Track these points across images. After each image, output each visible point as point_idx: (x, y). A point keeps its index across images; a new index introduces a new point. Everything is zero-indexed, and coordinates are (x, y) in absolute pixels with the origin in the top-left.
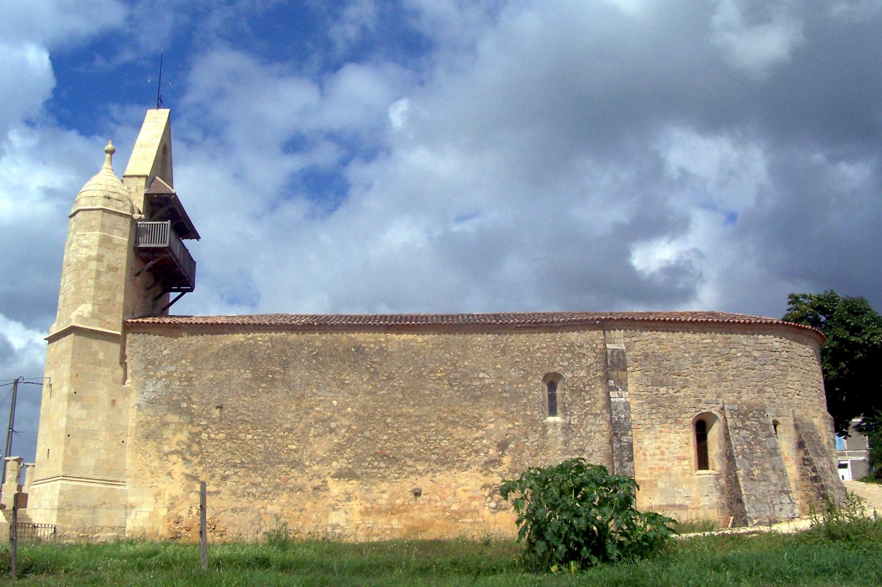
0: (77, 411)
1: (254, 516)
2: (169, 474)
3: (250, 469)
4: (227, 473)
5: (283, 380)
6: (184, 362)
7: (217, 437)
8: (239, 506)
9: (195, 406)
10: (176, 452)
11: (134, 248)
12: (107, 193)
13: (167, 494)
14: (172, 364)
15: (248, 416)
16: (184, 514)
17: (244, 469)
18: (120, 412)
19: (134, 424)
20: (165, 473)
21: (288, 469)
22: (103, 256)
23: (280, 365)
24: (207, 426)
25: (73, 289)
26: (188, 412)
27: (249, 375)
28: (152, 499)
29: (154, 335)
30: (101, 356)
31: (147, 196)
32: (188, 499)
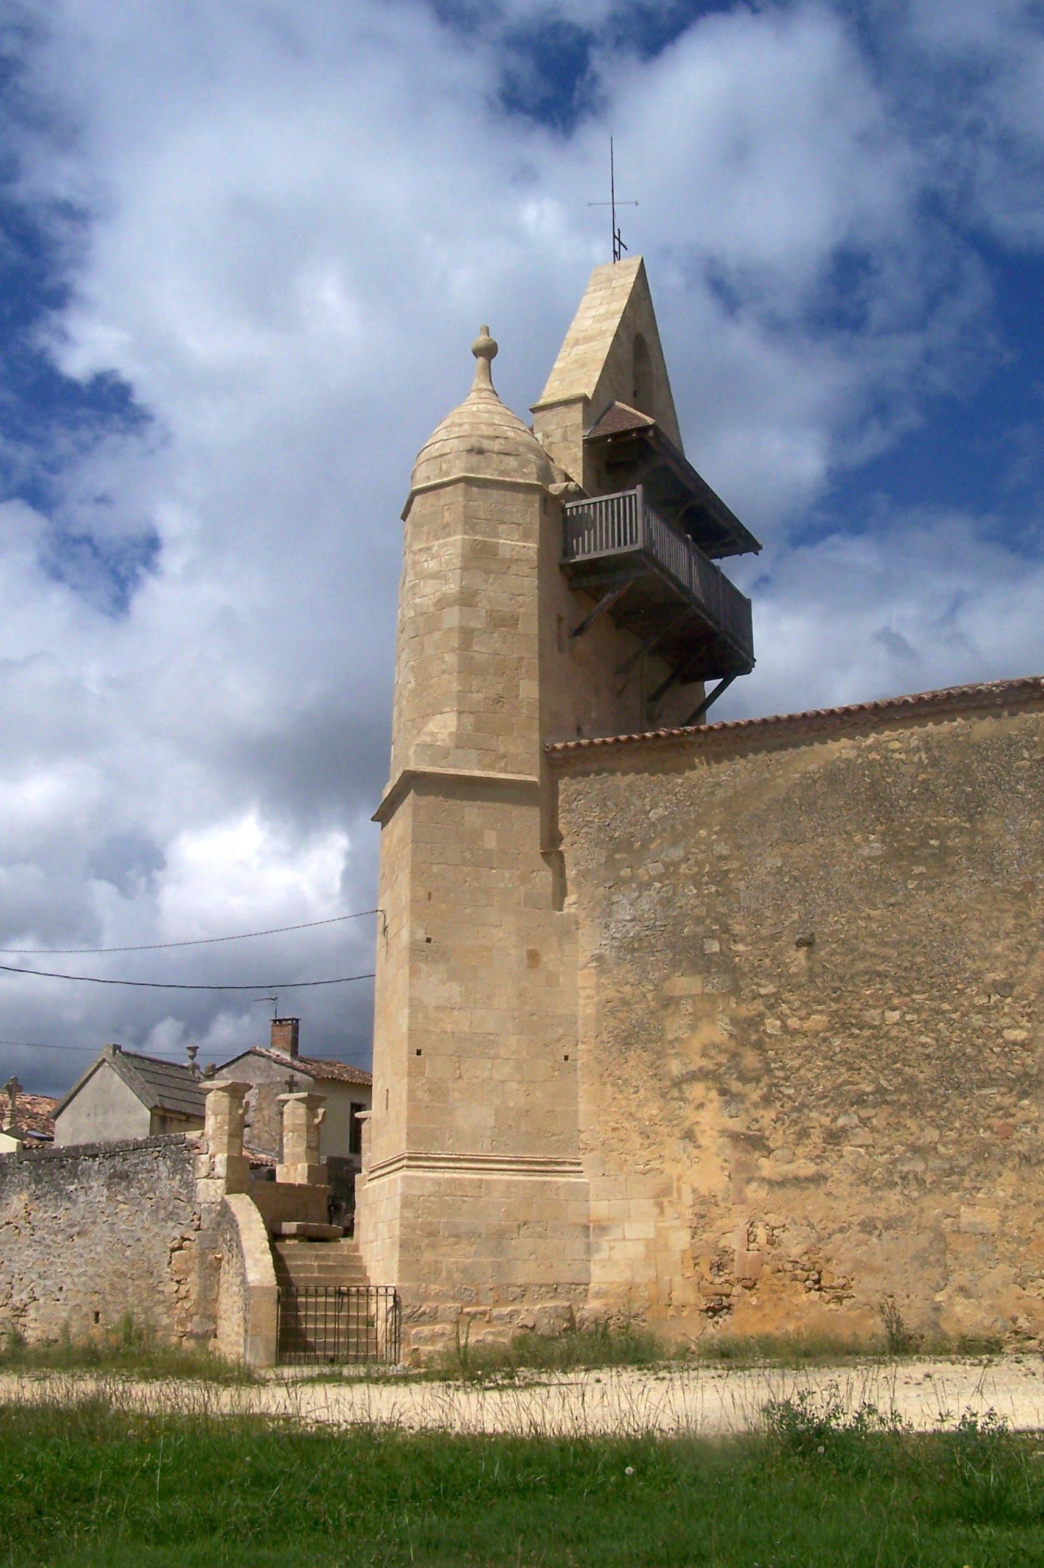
0: (438, 988)
1: (924, 1239)
2: (689, 1136)
3: (903, 1106)
4: (841, 1122)
5: (969, 849)
6: (703, 833)
7: (806, 1025)
8: (882, 1214)
9: (741, 947)
10: (702, 1075)
11: (562, 567)
12: (473, 442)
13: (686, 1190)
14: (674, 844)
15: (885, 959)
16: (734, 1242)
17: (887, 1109)
18: (551, 981)
19: (590, 1010)
20: (677, 1132)
21: (1008, 1101)
22: (476, 592)
23: (957, 809)
24: (777, 995)
25: (413, 684)
26: (726, 964)
27: (876, 847)
28: (647, 1205)
29: (625, 773)
30: (491, 841)
31: (590, 444)
32: (743, 1201)
